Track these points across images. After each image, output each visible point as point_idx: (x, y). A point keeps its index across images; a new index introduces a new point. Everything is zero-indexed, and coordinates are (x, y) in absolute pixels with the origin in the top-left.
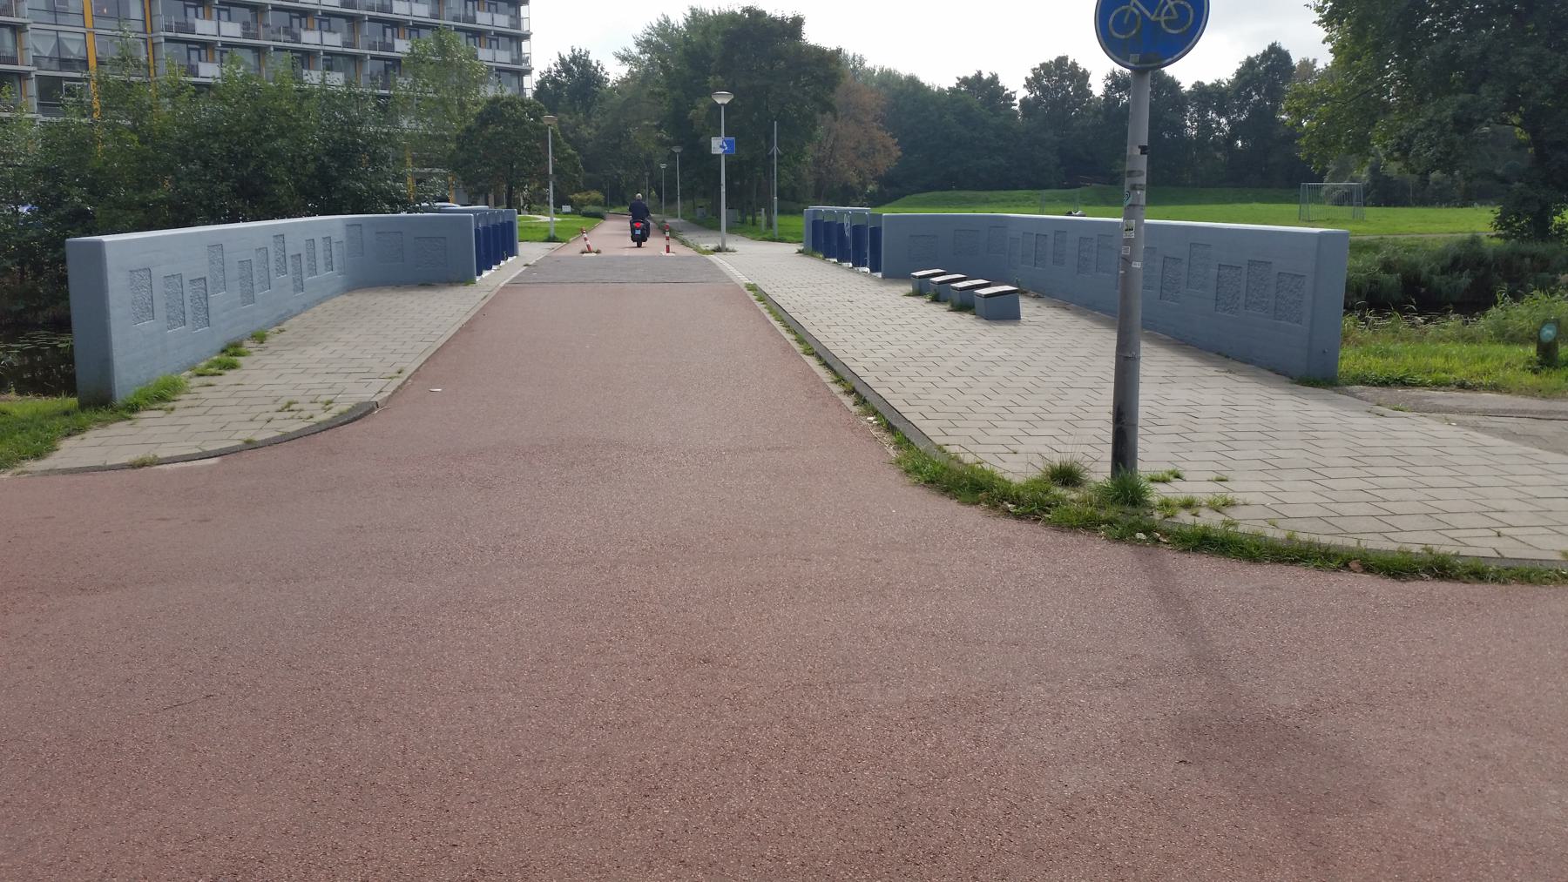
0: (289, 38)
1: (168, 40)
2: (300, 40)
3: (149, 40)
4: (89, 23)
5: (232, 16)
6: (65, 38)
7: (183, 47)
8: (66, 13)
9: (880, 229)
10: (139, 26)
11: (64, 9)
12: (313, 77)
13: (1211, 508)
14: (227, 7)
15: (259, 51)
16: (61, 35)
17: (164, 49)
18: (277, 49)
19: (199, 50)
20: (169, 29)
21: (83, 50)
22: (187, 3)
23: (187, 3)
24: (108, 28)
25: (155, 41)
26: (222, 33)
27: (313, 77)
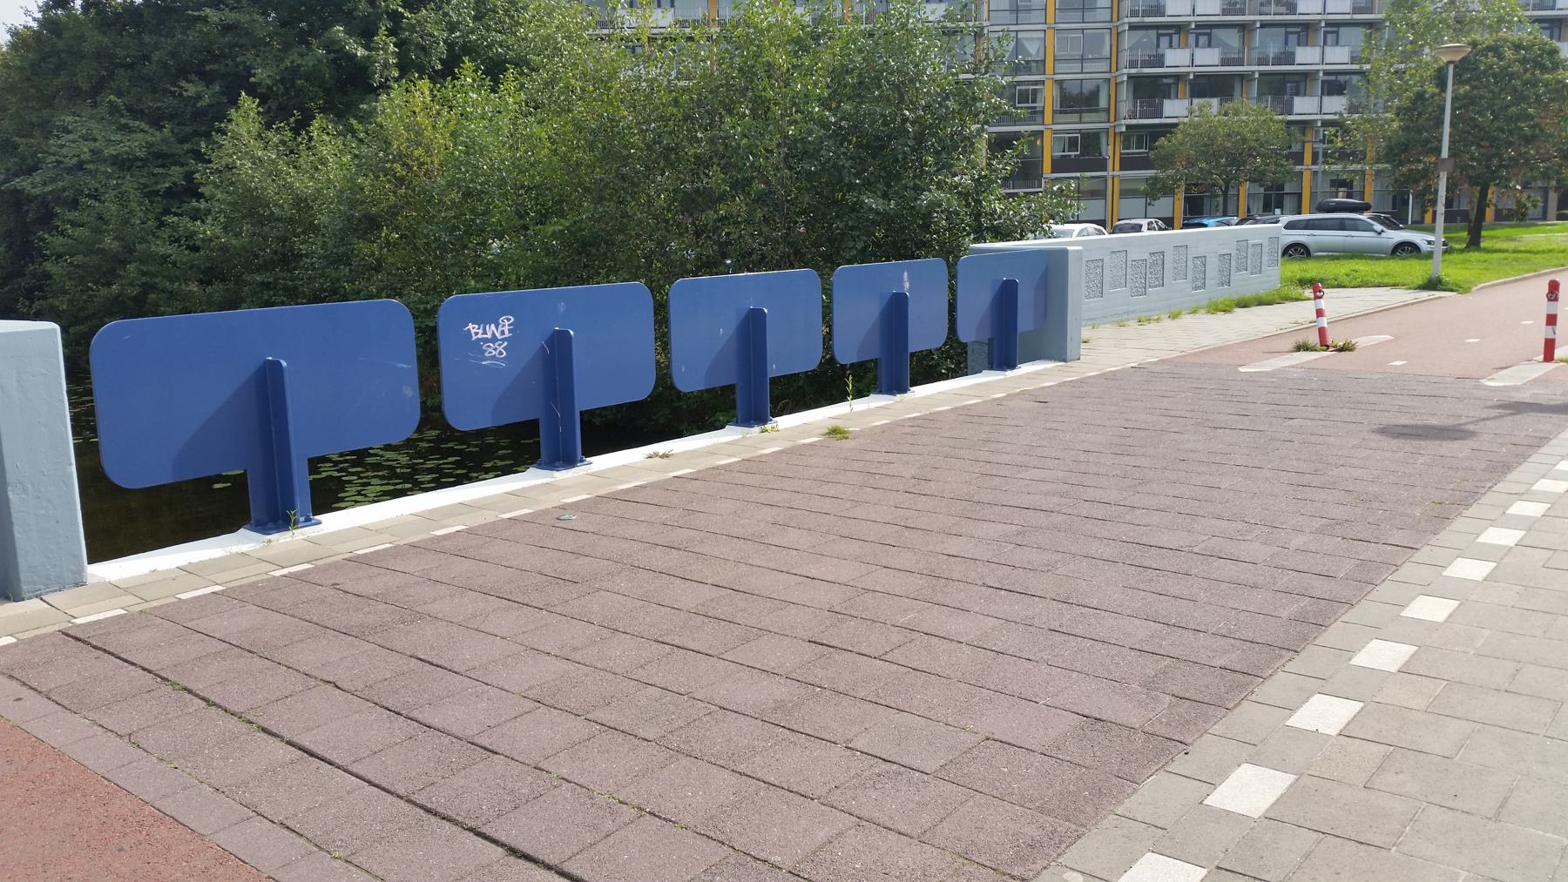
0: (1282, 9)
1: (1133, 27)
2: (1294, 61)
3: (1113, 81)
4: (1050, 19)
5: (1212, 42)
6: (1027, 39)
7: (1153, 33)
8: (1029, 10)
9: (18, 598)
10: (1105, 15)
11: (1027, 6)
12: (1305, 106)
13: (845, 432)
14: (1209, 31)
15: (1244, 27)
16: (1021, 35)
17: (1128, 40)
18: (1264, 25)
19: (1170, 35)
20: (1134, 13)
21: (1042, 54)
22: (1160, 32)
23: (1160, 32)
24: (1072, 22)
25: (1120, 29)
26: (1198, 11)
27: (1305, 106)
